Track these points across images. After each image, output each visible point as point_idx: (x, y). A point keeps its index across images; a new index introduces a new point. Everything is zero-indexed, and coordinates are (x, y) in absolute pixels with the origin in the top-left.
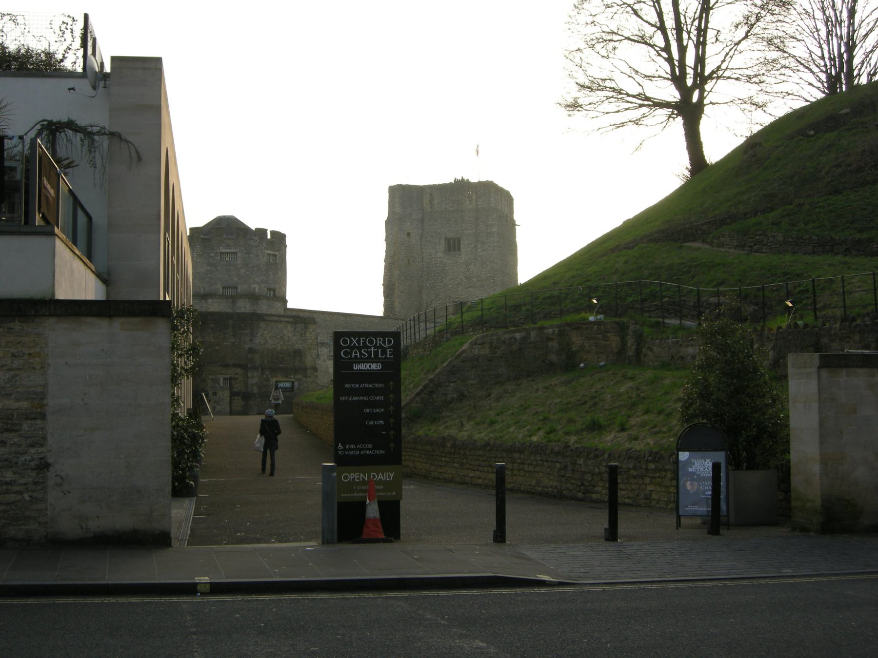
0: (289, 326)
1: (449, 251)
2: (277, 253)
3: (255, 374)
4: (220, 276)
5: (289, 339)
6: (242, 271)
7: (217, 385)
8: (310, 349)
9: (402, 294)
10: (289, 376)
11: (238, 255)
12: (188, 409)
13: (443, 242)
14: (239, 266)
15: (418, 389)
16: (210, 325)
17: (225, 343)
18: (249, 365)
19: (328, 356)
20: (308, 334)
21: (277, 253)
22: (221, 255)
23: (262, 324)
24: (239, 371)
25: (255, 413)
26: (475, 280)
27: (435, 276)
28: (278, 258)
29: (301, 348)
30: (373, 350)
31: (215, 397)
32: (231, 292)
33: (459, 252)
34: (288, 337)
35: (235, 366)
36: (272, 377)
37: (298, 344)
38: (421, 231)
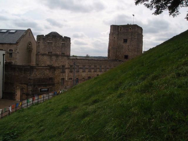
1: (124, 42)
3: (31, 87)
8: (56, 77)
20: (55, 72)
23: (35, 70)
24: (26, 86)
32: (50, 54)
35: (24, 84)
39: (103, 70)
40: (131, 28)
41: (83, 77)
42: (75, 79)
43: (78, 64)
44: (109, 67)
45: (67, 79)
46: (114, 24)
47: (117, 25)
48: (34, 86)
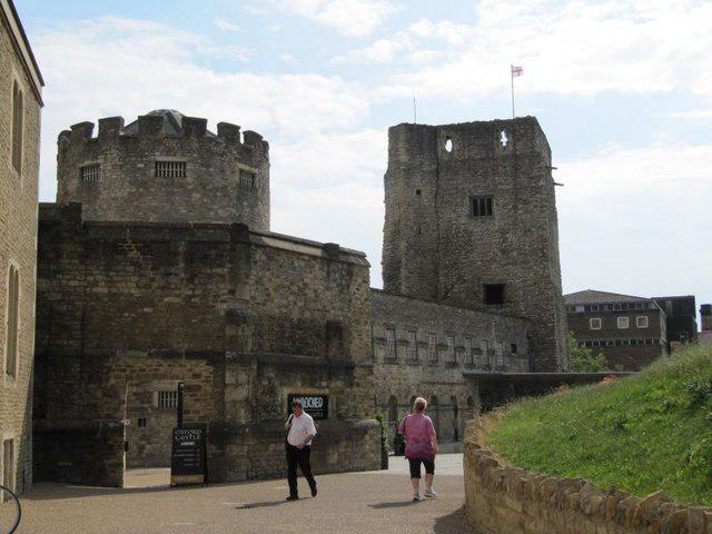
0: (317, 267)
1: (476, 213)
2: (256, 171)
3: (243, 377)
4: (154, 204)
5: (316, 296)
6: (196, 196)
7: (146, 405)
8: (358, 322)
10: (317, 384)
11: (188, 167)
12: (207, 364)
13: (467, 201)
14: (190, 187)
16: (131, 255)
17: (166, 300)
18: (229, 355)
21: (256, 171)
22: (156, 167)
24: (203, 368)
25: (244, 476)
26: (515, 253)
29: (341, 318)
31: (142, 428)
34: (315, 291)
35: (191, 355)
36: (281, 384)
37: (333, 308)
46: (411, 122)
47: (425, 126)
48: (262, 365)
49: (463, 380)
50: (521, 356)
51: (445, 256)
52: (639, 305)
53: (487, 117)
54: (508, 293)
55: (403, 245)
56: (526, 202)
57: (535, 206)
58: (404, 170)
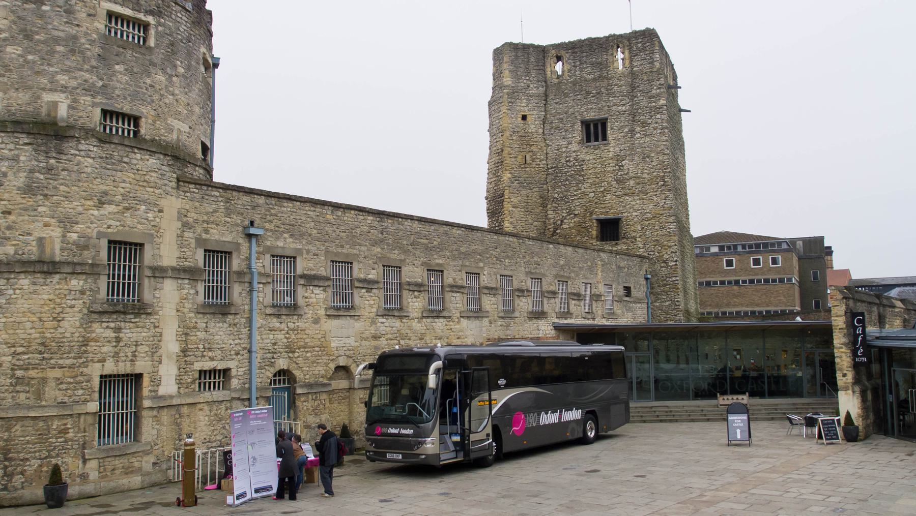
1: (588, 140)
2: (150, 19)
9: (514, 210)
13: (578, 126)
15: (511, 239)
19: (326, 309)
27: (567, 180)
28: (152, 32)
30: (772, 380)
33: (605, 142)
38: (543, 113)
39: (489, 303)
40: (612, 46)
41: (342, 362)
42: (262, 377)
43: (286, 244)
44: (529, 284)
45: (168, 387)
47: (532, 46)
49: (553, 333)
50: (639, 301)
51: (554, 188)
52: (773, 245)
53: (601, 32)
54: (624, 228)
55: (507, 176)
56: (644, 124)
57: (655, 129)
58: (508, 94)
